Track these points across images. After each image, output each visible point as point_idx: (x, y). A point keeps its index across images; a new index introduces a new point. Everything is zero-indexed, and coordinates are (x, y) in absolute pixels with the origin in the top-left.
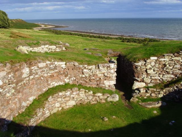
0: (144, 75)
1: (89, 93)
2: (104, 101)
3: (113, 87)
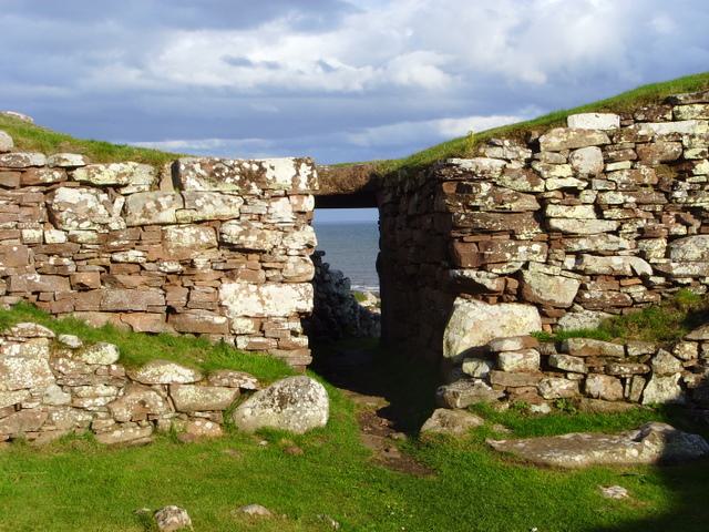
0: (522, 249)
1: (90, 357)
2: (210, 428)
3: (294, 333)
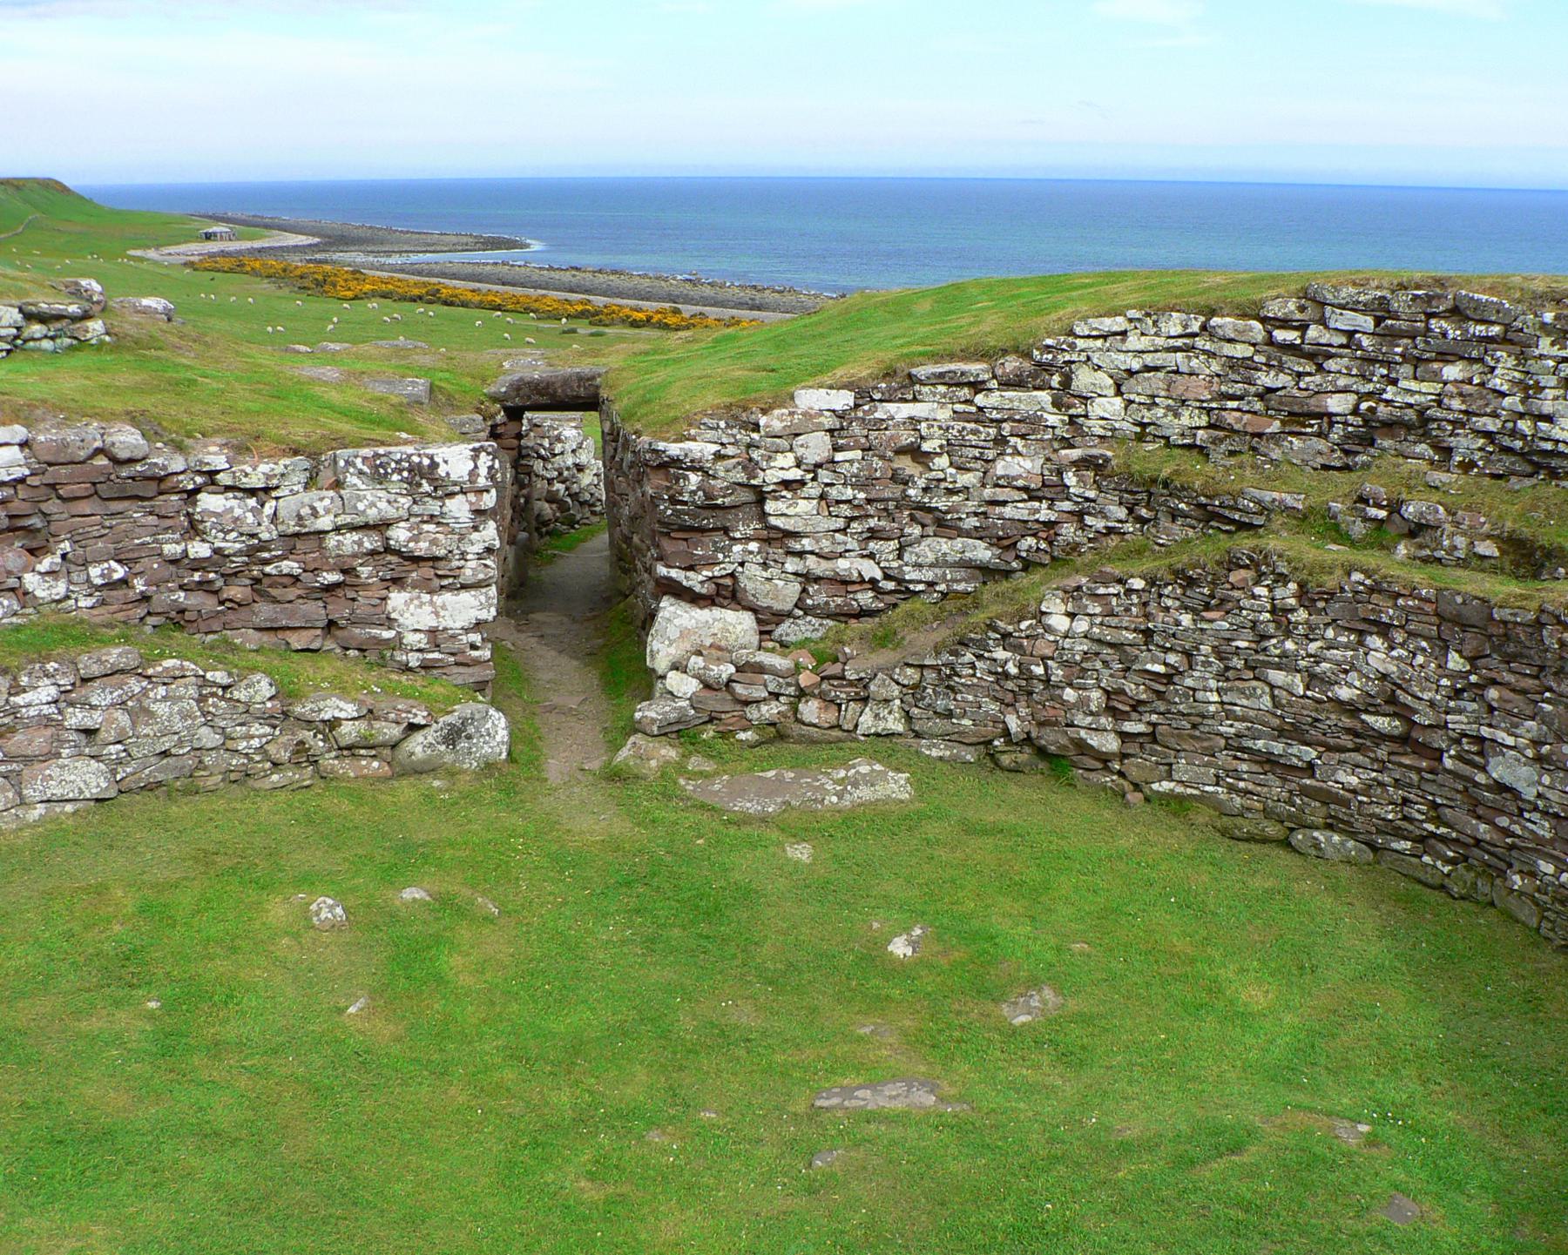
3: (473, 647)
